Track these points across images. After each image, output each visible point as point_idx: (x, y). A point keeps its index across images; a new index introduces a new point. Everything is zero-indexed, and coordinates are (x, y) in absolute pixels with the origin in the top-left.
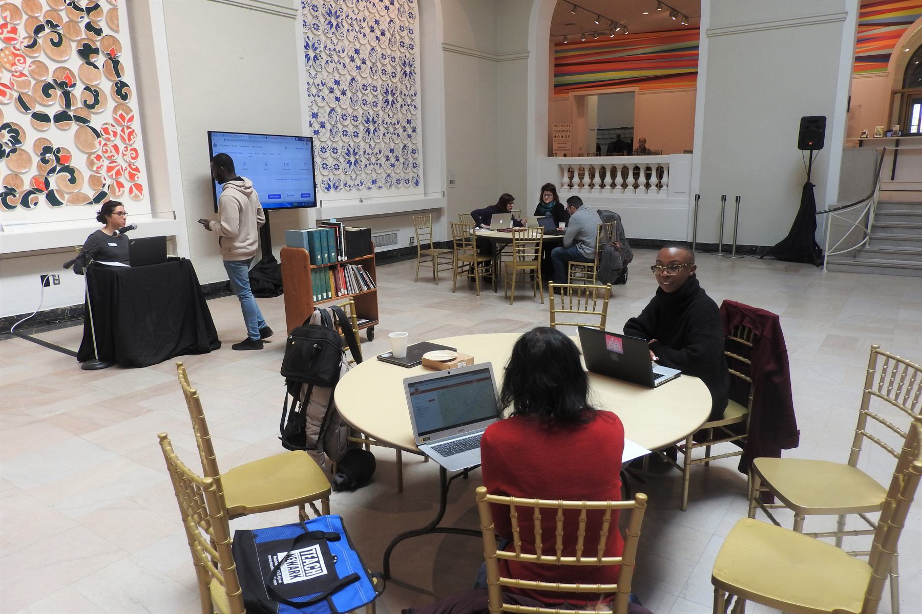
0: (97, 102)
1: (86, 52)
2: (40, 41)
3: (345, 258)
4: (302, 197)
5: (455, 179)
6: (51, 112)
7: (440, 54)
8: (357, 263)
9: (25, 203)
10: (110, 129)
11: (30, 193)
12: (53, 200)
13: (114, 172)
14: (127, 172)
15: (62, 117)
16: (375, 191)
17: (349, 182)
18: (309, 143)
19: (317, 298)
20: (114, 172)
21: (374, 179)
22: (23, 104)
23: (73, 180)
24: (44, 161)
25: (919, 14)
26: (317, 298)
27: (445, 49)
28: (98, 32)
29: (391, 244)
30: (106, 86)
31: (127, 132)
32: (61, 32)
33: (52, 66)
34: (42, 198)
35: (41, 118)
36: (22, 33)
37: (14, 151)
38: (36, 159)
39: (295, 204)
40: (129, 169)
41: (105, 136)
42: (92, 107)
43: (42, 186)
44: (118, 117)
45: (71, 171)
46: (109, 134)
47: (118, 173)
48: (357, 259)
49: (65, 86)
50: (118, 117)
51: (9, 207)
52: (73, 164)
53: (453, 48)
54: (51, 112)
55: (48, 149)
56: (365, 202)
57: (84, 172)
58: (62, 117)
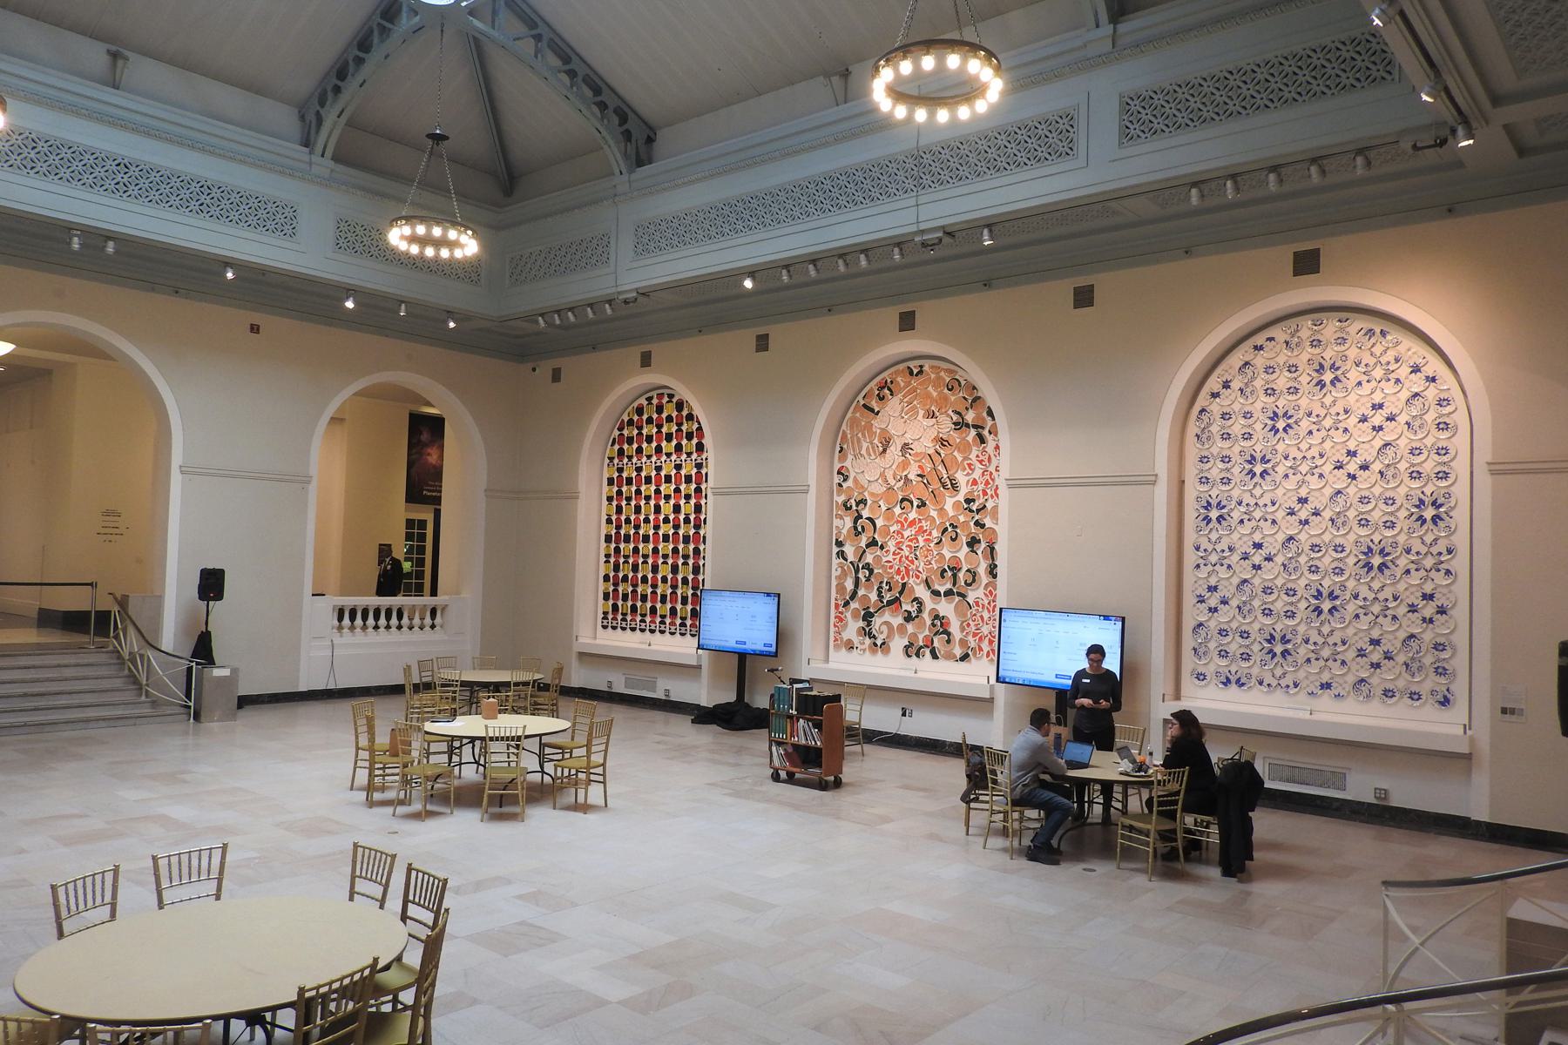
0: (974, 581)
1: (973, 543)
2: (943, 539)
3: (794, 712)
4: (1057, 677)
5: (1522, 707)
6: (942, 590)
7: (1488, 479)
8: (808, 720)
9: (918, 655)
10: (981, 602)
11: (921, 647)
12: (935, 656)
13: (977, 638)
14: (987, 638)
15: (949, 593)
16: (1326, 700)
17: (1268, 679)
18: (776, 598)
19: (775, 735)
20: (977, 638)
21: (1324, 682)
22: (927, 583)
23: (948, 641)
24: (934, 625)
25: (636, 160)
26: (775, 735)
27: (1493, 473)
28: (983, 526)
29: (1329, 787)
30: (982, 570)
31: (992, 604)
32: (958, 531)
33: (948, 555)
34: (927, 651)
35: (936, 593)
36: (935, 534)
37: (917, 617)
38: (929, 622)
39: (758, 652)
40: (989, 636)
41: (976, 608)
42: (970, 585)
43: (929, 644)
44: (987, 593)
45: (949, 634)
46: (979, 606)
47: (981, 639)
48: (808, 716)
49: (955, 570)
50: (987, 593)
51: (909, 656)
52: (951, 630)
53: (1512, 467)
54: (942, 590)
55: (937, 617)
56: (920, 675)
57: (957, 634)
58: (949, 593)
